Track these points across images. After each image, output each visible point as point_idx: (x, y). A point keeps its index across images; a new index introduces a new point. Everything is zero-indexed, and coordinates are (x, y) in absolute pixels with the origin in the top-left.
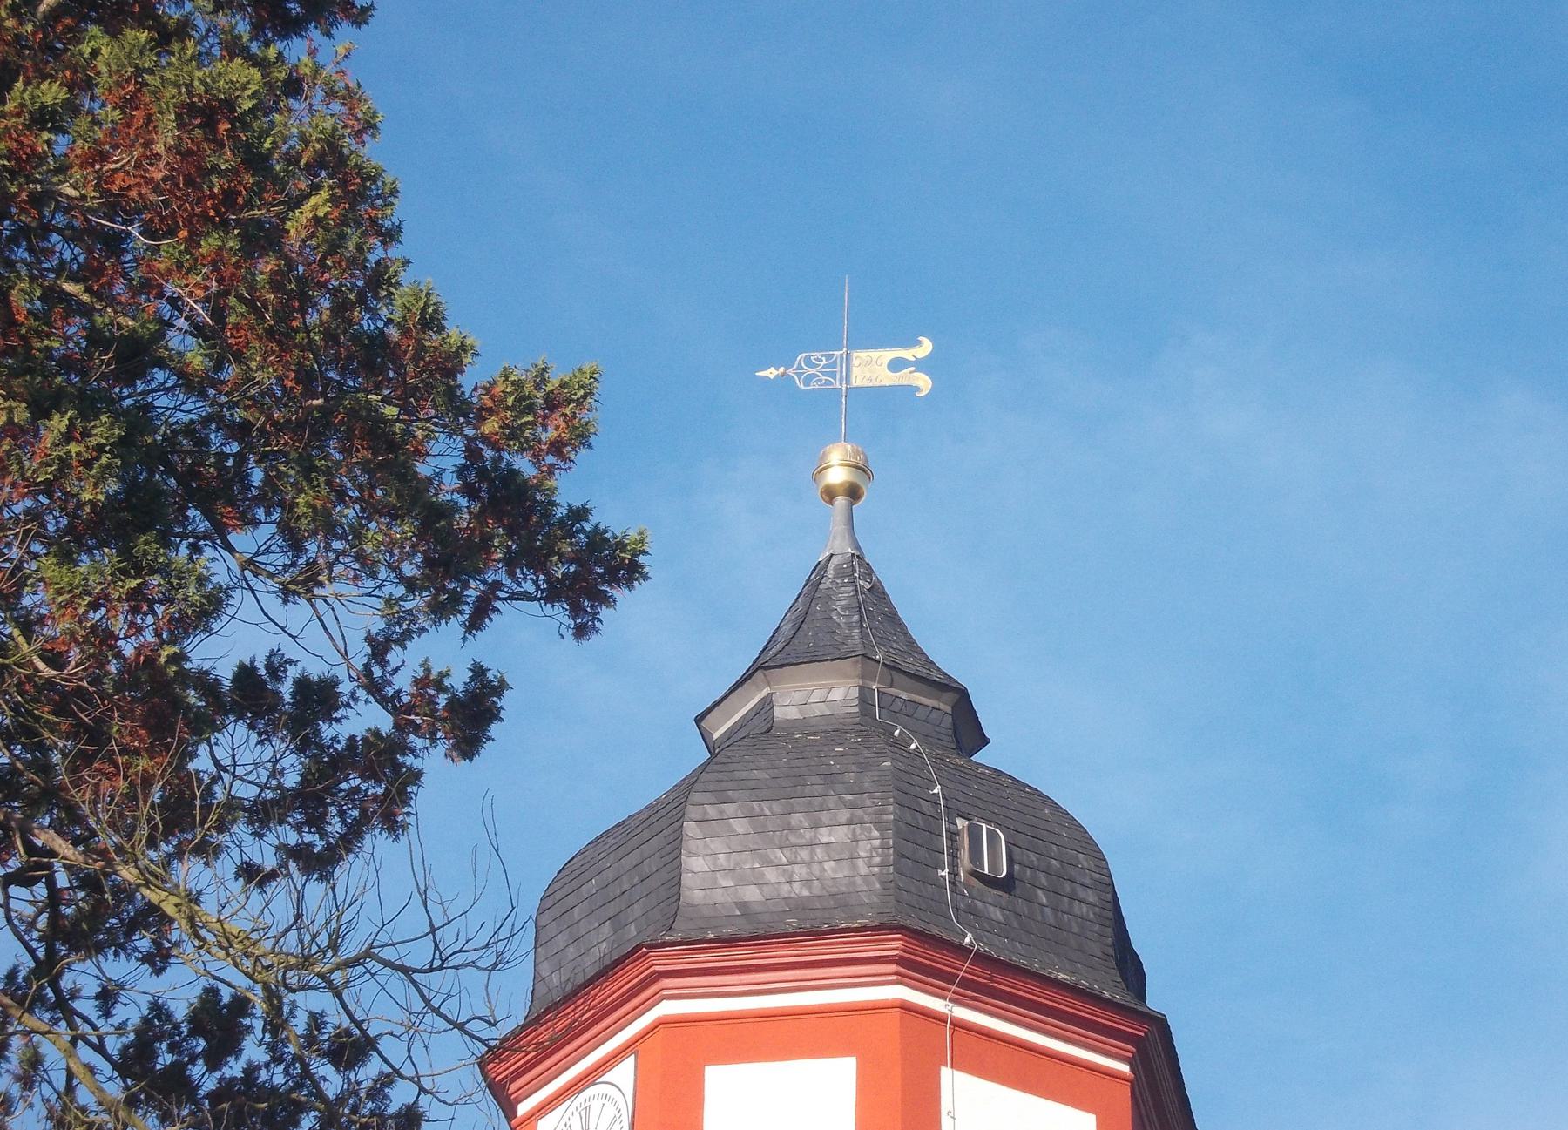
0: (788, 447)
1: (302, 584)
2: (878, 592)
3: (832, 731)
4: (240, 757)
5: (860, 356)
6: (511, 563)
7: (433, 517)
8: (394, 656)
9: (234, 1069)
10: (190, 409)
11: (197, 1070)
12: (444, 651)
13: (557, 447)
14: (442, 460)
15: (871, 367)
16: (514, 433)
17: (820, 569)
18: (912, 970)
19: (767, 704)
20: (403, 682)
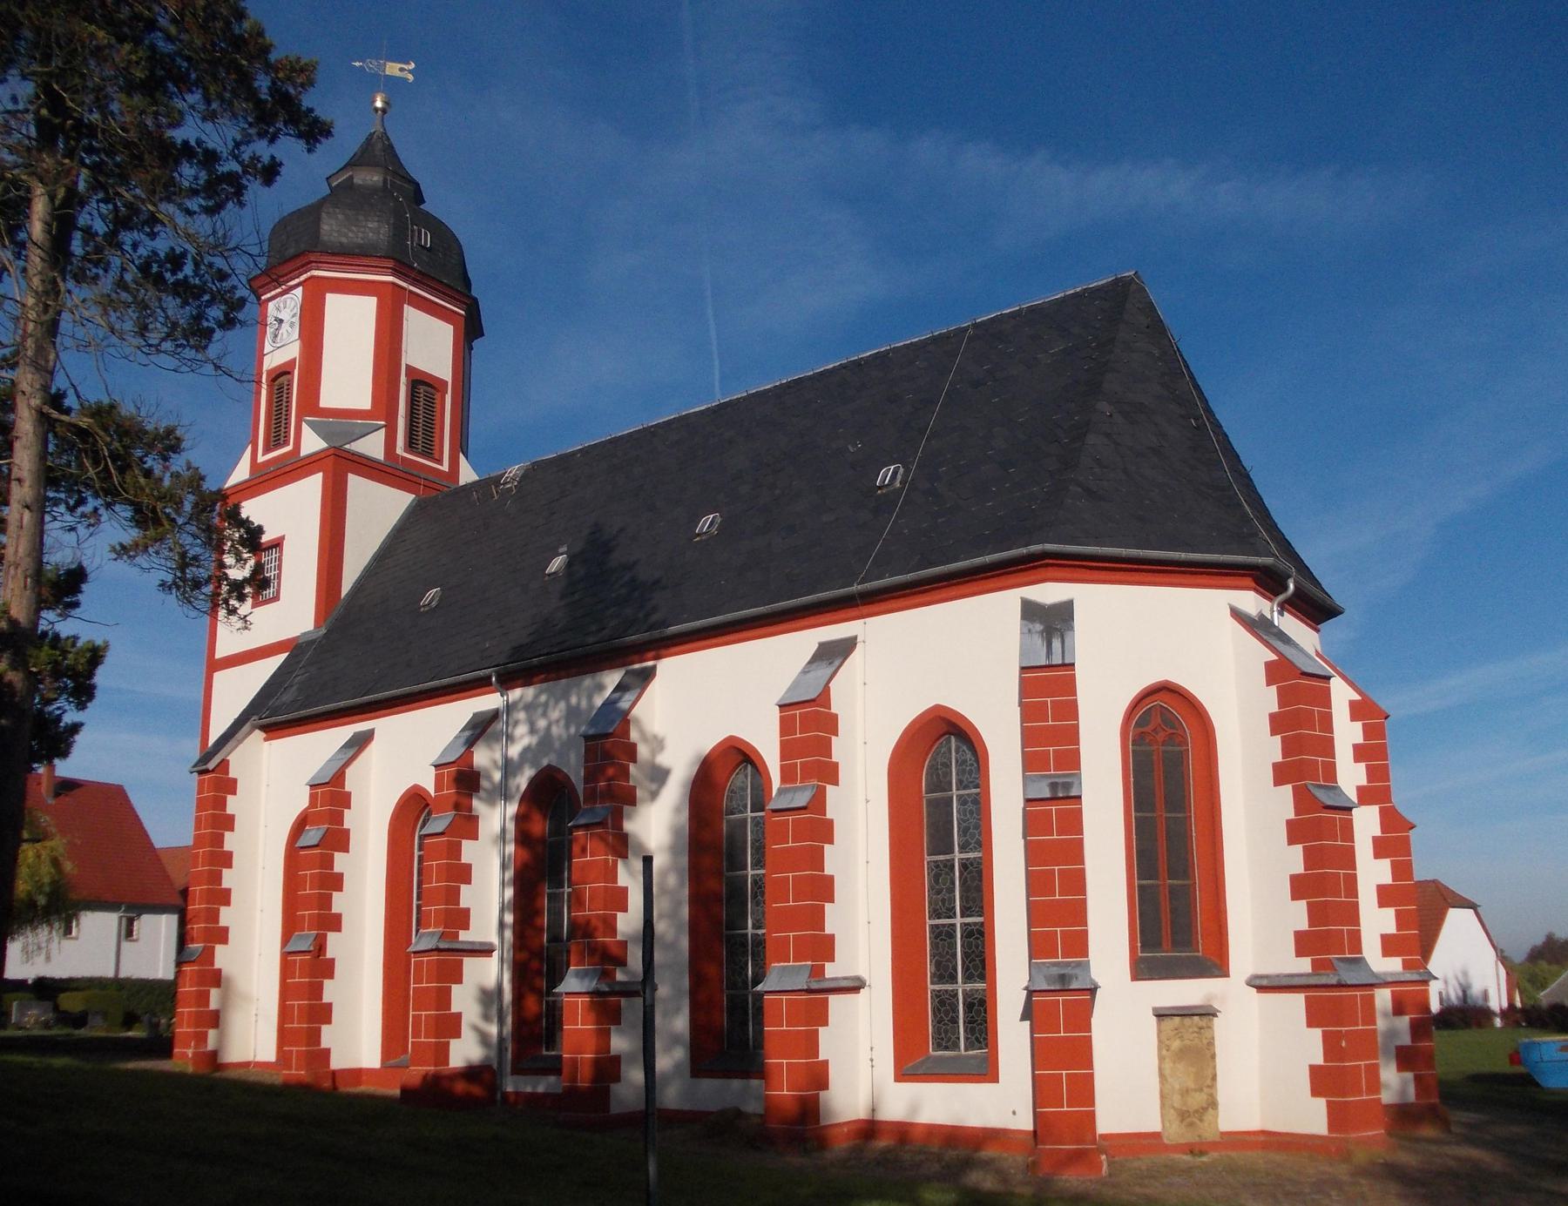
0: (373, 91)
1: (210, 116)
2: (391, 147)
3: (373, 190)
4: (188, 172)
5: (389, 64)
6: (285, 124)
7: (259, 103)
8: (243, 148)
9: (180, 276)
10: (170, 48)
11: (168, 275)
12: (262, 150)
13: (302, 85)
14: (263, 83)
15: (393, 69)
16: (289, 78)
17: (372, 135)
18: (396, 272)
19: (351, 177)
20: (246, 157)
